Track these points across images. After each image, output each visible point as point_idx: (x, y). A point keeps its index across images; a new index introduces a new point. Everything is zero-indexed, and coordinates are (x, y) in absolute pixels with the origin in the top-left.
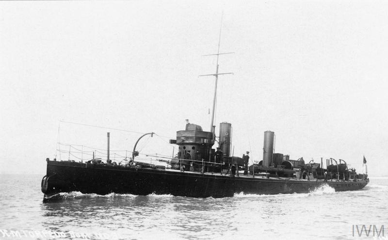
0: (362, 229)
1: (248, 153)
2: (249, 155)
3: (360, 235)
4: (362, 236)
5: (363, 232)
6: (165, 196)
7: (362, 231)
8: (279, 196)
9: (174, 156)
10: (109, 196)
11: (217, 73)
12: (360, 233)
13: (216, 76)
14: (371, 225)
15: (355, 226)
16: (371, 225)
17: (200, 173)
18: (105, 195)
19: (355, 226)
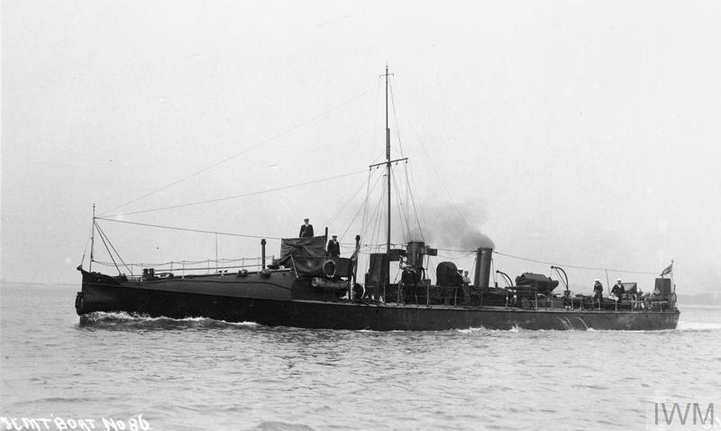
0: (672, 415)
1: (307, 221)
2: (310, 223)
3: (669, 422)
4: (672, 423)
5: (671, 409)
6: (251, 323)
7: (673, 412)
8: (428, 338)
9: (269, 262)
10: (198, 319)
11: (388, 156)
12: (669, 415)
13: (389, 164)
14: (689, 404)
15: (660, 407)
16: (689, 404)
17: (424, 307)
18: (119, 312)
19: (660, 407)
